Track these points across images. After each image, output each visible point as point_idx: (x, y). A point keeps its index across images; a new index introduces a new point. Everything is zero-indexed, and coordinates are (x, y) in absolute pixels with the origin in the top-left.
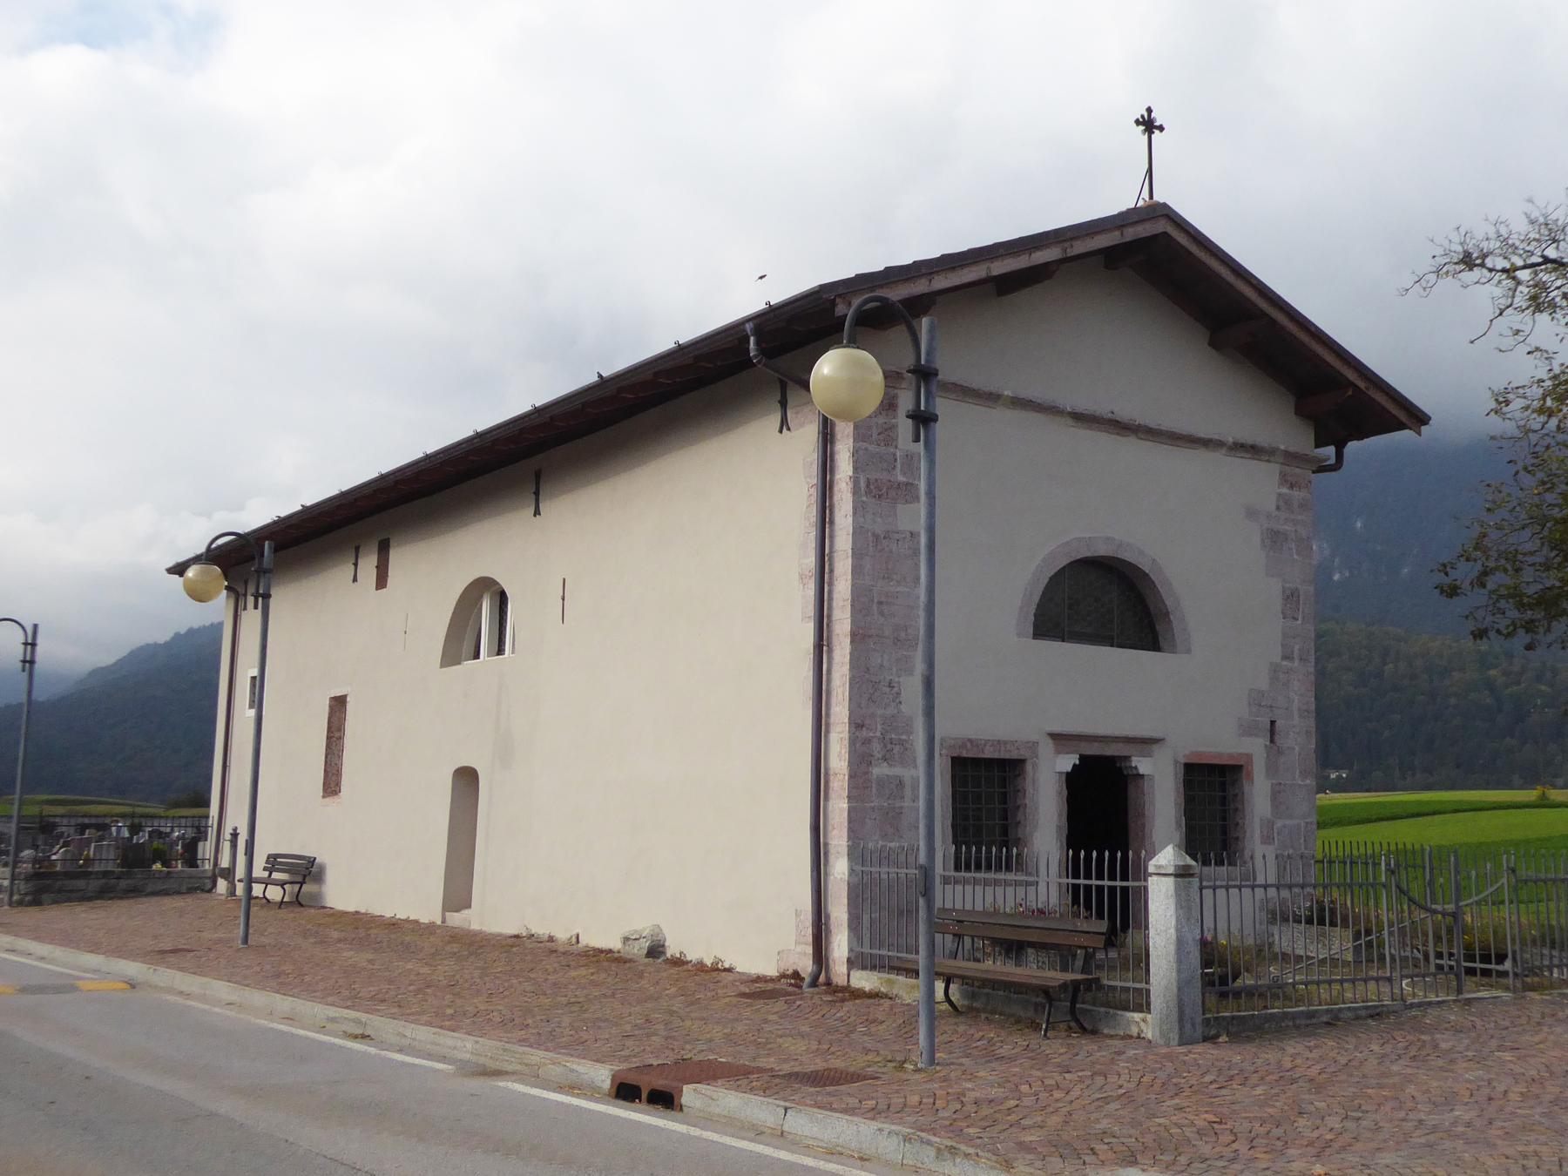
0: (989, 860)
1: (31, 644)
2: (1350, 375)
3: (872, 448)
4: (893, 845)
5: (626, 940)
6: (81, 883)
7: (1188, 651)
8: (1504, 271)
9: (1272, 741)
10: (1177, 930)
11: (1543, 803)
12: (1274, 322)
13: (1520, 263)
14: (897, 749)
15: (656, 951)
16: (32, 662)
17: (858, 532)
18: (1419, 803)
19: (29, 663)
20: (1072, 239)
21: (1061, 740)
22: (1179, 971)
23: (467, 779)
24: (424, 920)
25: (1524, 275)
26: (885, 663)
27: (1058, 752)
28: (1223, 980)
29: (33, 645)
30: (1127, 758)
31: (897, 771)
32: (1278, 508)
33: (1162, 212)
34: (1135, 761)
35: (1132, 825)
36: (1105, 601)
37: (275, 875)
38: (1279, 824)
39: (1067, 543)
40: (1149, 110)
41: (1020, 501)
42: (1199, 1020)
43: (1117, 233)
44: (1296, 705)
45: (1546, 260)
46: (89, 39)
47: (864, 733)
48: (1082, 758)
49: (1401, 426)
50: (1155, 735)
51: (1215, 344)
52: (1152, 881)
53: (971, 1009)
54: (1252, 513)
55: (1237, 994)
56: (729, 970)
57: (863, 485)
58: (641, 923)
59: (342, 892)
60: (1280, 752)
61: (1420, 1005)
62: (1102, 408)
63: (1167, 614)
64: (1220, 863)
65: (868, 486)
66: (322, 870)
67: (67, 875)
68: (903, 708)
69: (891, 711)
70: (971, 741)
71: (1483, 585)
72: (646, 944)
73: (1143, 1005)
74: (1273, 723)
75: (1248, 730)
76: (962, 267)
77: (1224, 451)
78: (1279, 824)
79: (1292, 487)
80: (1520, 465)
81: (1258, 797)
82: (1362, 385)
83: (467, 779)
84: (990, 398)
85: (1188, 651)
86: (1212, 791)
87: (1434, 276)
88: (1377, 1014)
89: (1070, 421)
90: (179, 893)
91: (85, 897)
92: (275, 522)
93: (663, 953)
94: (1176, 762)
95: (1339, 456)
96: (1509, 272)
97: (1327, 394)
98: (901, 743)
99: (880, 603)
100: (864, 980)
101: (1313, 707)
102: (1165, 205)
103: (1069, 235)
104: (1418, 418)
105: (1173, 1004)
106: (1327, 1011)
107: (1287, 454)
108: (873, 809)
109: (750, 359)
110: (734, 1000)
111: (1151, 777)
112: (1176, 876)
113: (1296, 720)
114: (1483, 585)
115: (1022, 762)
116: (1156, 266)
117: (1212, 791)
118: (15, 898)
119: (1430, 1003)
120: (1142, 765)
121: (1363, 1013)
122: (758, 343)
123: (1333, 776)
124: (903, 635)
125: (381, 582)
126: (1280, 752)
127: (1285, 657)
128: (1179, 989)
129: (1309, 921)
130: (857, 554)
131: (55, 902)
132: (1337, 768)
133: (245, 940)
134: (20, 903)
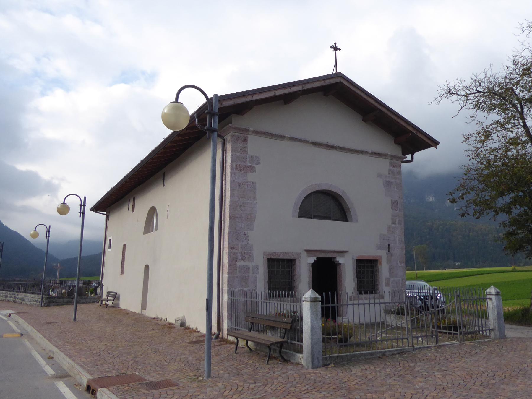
0: (273, 294)
1: (48, 231)
2: (411, 129)
3: (238, 154)
4: (245, 289)
5: (176, 320)
6: (61, 300)
7: (357, 221)
8: (464, 95)
9: (389, 251)
10: (311, 323)
11: (514, 271)
12: (381, 111)
13: (469, 93)
14: (247, 256)
15: (183, 324)
16: (49, 236)
17: (232, 182)
18: (463, 272)
19: (48, 237)
20: (306, 83)
21: (309, 252)
22: (312, 339)
23: (147, 267)
24: (137, 312)
25: (471, 97)
26: (243, 227)
27: (308, 256)
28: (346, 340)
29: (49, 231)
30: (335, 258)
31: (247, 263)
32: (389, 174)
33: (339, 75)
34: (338, 259)
35: (338, 281)
36: (326, 205)
37: (109, 298)
38: (392, 279)
39: (311, 186)
40: (335, 44)
41: (287, 170)
42: (321, 358)
43: (323, 82)
44: (397, 239)
45: (478, 92)
46: (125, 81)
47: (234, 251)
48: (317, 258)
49: (429, 146)
50: (345, 250)
51: (364, 120)
52: (304, 303)
53: (256, 349)
54: (379, 175)
55: (352, 345)
56: (198, 332)
57: (234, 166)
58: (180, 316)
59: (123, 305)
60: (392, 255)
61: (420, 348)
62: (324, 141)
63: (349, 209)
64: (372, 293)
65: (236, 167)
66: (119, 296)
67: (58, 298)
68: (249, 242)
69: (245, 242)
70: (275, 253)
71: (463, 198)
72: (179, 322)
73: (302, 352)
74: (389, 245)
75: (380, 248)
76: (265, 92)
77: (369, 155)
78: (392, 279)
79: (394, 167)
80: (471, 157)
81: (384, 271)
82: (414, 132)
83: (147, 267)
84: (282, 137)
85: (357, 221)
86: (367, 269)
87: (440, 98)
88: (401, 353)
89: (311, 145)
90: (90, 303)
91: (62, 304)
92: (107, 194)
93: (185, 325)
94: (353, 259)
95: (412, 157)
96: (466, 95)
97: (409, 138)
98: (249, 254)
99: (241, 206)
100: (231, 339)
101: (404, 240)
102: (340, 73)
103: (305, 82)
104: (435, 143)
105: (310, 352)
106: (380, 352)
107: (391, 156)
108: (237, 277)
109: (196, 126)
110: (187, 344)
111: (344, 264)
112: (311, 301)
113: (398, 244)
114: (463, 198)
115: (295, 260)
116: (337, 92)
117: (367, 269)
118: (43, 304)
119: (424, 348)
120: (340, 260)
121: (396, 352)
122: (198, 120)
123: (457, 264)
124: (249, 217)
125: (133, 210)
126: (392, 255)
127: (393, 223)
128: (312, 346)
129: (398, 313)
130: (232, 189)
131: (54, 306)
132: (458, 262)
133: (75, 319)
134: (44, 306)
